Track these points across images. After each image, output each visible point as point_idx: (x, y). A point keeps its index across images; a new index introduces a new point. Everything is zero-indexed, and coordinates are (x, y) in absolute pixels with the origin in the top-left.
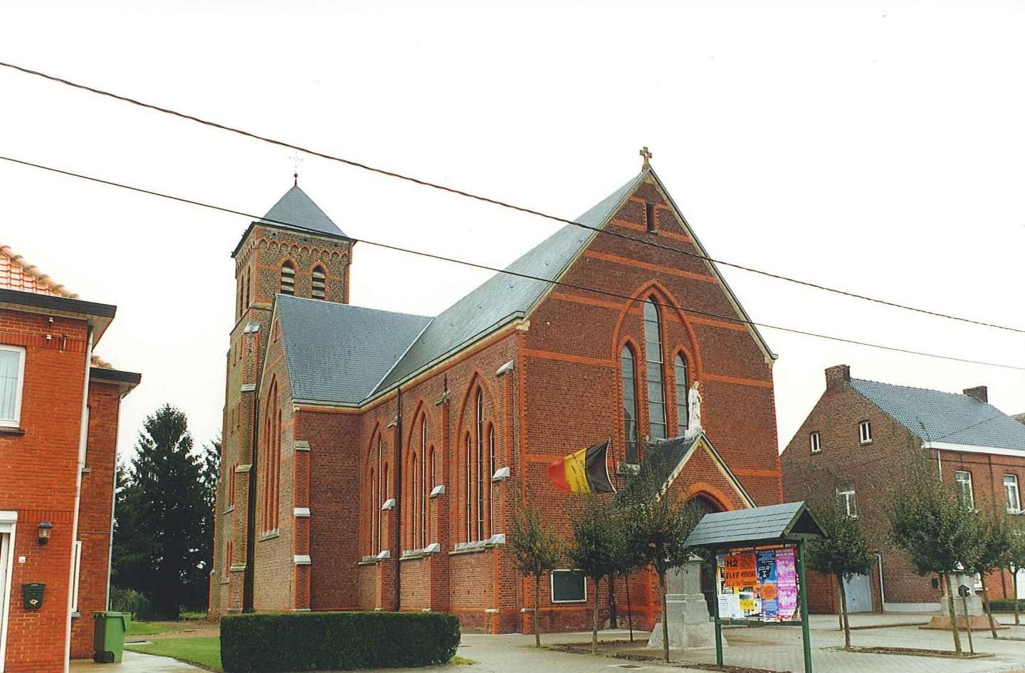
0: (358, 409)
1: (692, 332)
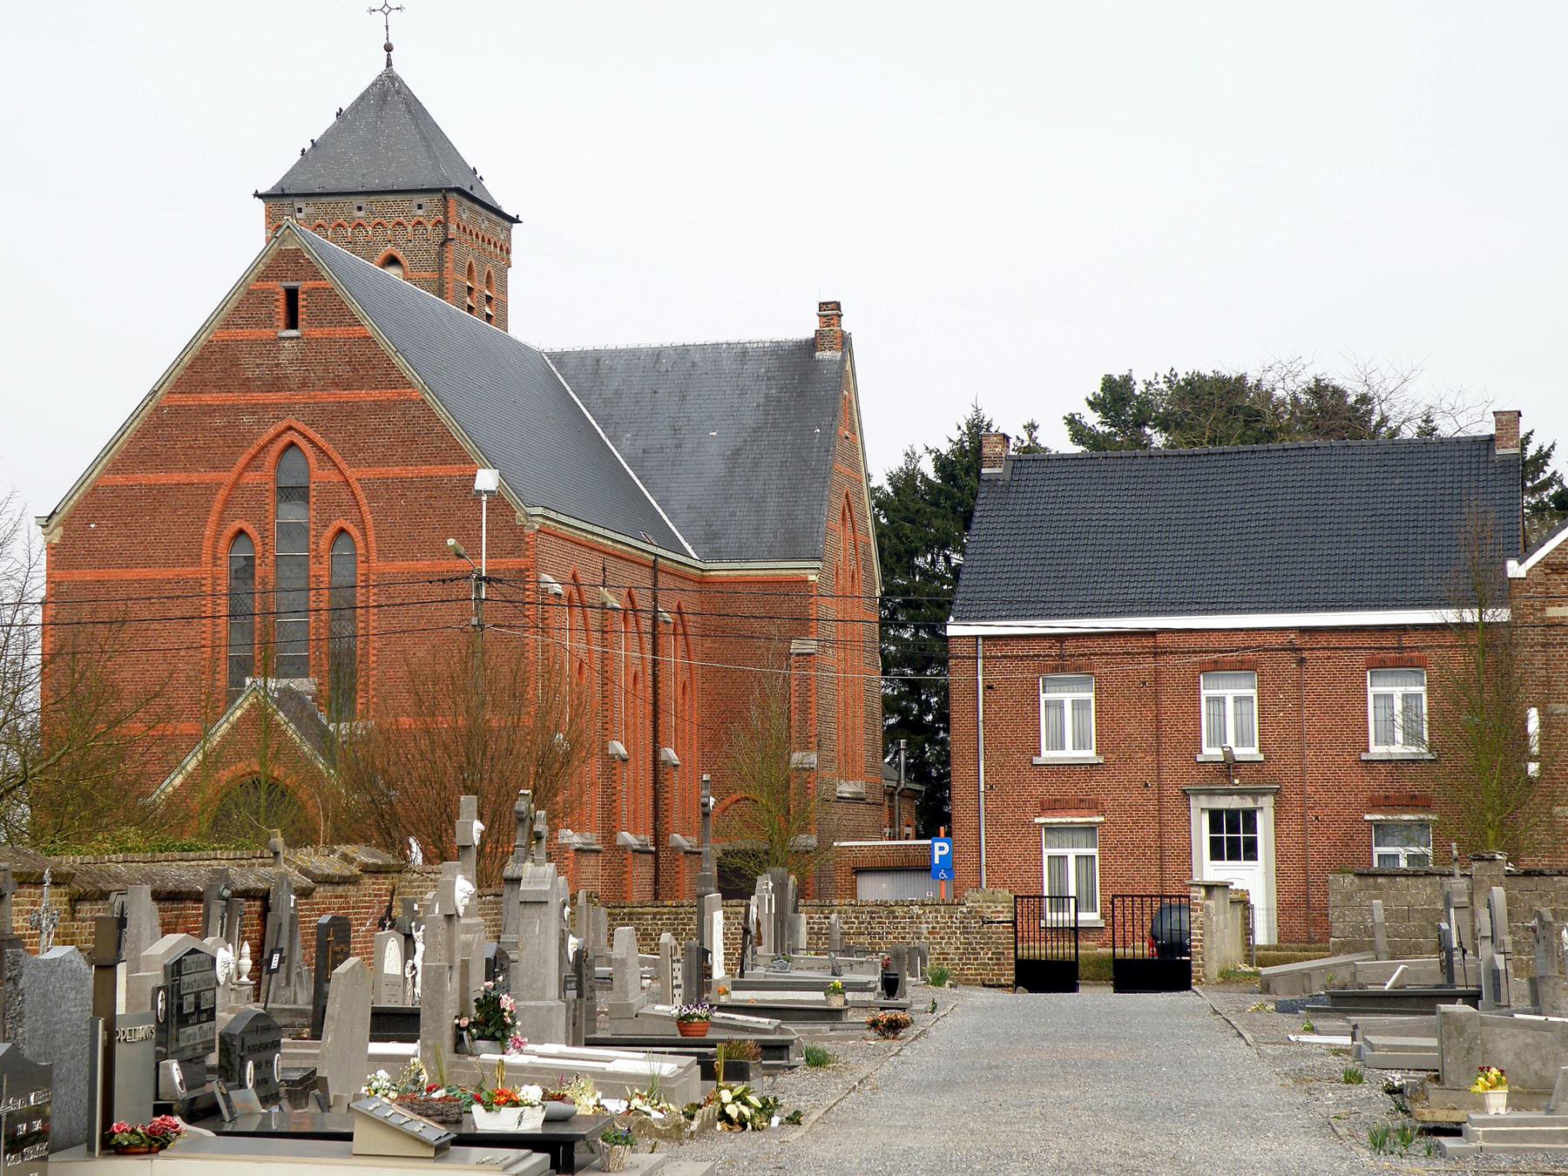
0: (700, 572)
1: (361, 495)
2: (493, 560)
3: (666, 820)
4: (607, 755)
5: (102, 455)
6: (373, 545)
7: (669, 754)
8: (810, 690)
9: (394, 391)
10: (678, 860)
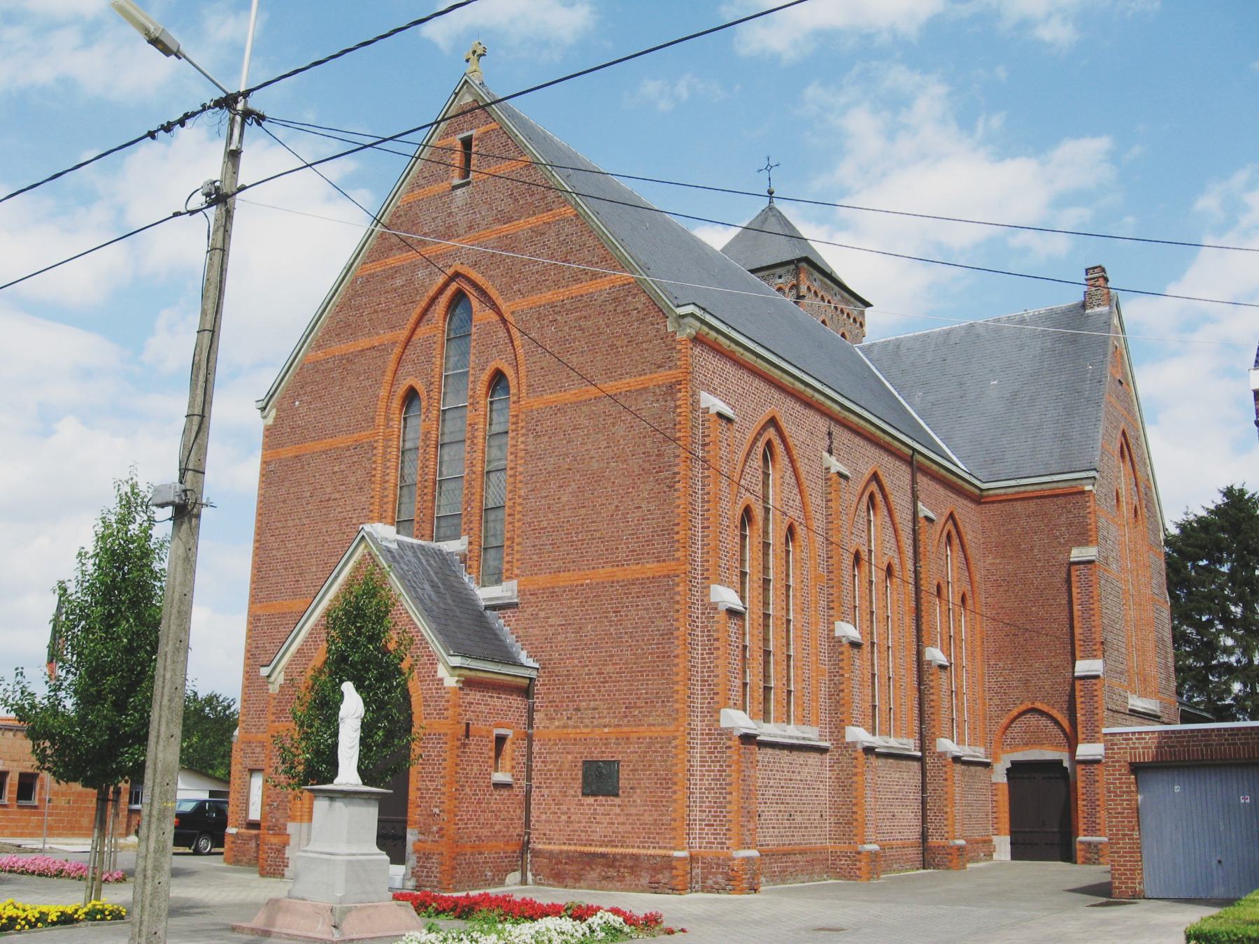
2: (642, 378)
3: (932, 723)
4: (833, 638)
5: (307, 333)
6: (523, 381)
7: (935, 654)
8: (1092, 597)
9: (549, 213)
10: (945, 766)
